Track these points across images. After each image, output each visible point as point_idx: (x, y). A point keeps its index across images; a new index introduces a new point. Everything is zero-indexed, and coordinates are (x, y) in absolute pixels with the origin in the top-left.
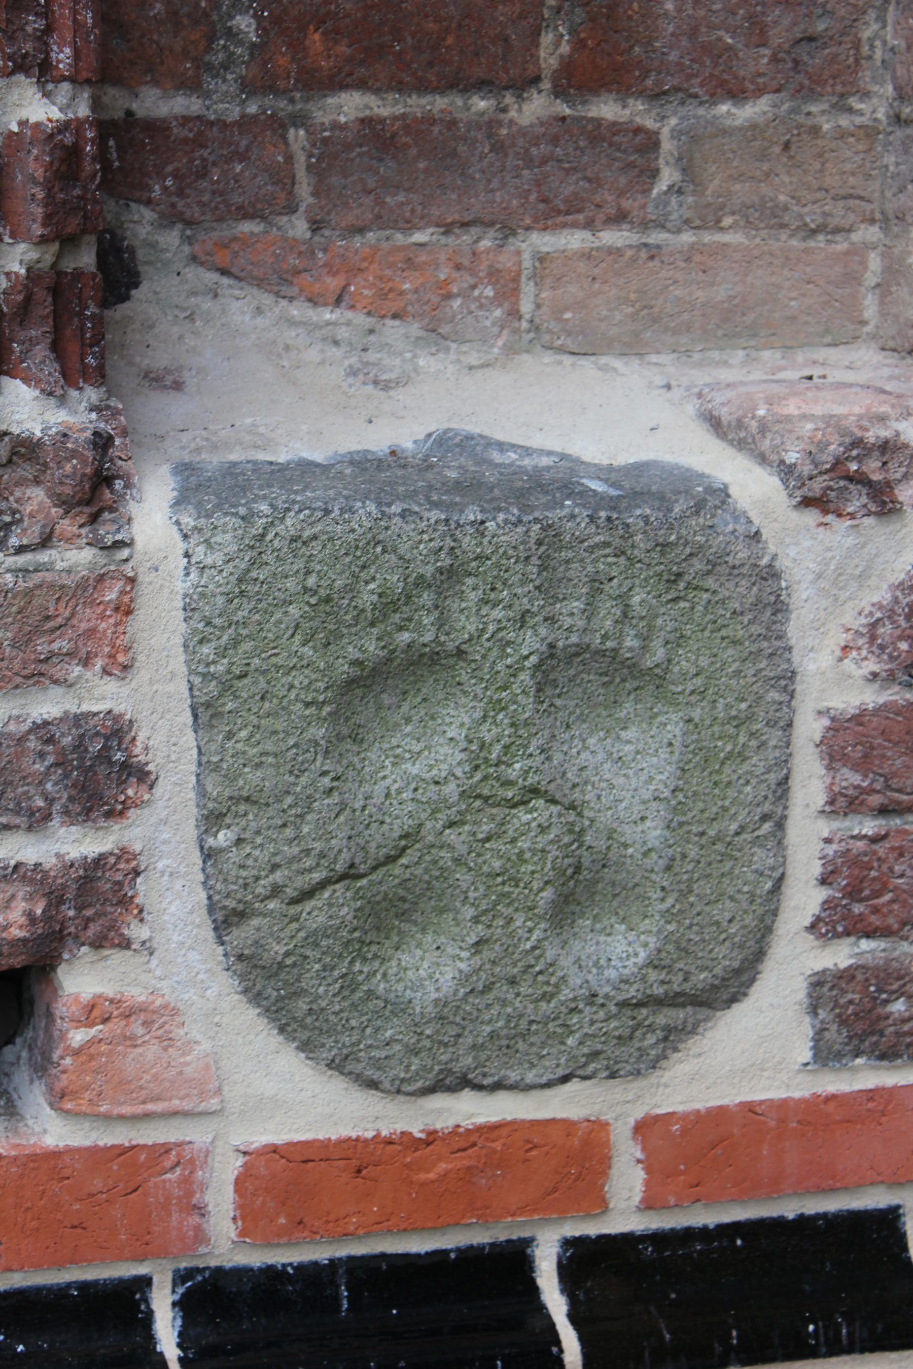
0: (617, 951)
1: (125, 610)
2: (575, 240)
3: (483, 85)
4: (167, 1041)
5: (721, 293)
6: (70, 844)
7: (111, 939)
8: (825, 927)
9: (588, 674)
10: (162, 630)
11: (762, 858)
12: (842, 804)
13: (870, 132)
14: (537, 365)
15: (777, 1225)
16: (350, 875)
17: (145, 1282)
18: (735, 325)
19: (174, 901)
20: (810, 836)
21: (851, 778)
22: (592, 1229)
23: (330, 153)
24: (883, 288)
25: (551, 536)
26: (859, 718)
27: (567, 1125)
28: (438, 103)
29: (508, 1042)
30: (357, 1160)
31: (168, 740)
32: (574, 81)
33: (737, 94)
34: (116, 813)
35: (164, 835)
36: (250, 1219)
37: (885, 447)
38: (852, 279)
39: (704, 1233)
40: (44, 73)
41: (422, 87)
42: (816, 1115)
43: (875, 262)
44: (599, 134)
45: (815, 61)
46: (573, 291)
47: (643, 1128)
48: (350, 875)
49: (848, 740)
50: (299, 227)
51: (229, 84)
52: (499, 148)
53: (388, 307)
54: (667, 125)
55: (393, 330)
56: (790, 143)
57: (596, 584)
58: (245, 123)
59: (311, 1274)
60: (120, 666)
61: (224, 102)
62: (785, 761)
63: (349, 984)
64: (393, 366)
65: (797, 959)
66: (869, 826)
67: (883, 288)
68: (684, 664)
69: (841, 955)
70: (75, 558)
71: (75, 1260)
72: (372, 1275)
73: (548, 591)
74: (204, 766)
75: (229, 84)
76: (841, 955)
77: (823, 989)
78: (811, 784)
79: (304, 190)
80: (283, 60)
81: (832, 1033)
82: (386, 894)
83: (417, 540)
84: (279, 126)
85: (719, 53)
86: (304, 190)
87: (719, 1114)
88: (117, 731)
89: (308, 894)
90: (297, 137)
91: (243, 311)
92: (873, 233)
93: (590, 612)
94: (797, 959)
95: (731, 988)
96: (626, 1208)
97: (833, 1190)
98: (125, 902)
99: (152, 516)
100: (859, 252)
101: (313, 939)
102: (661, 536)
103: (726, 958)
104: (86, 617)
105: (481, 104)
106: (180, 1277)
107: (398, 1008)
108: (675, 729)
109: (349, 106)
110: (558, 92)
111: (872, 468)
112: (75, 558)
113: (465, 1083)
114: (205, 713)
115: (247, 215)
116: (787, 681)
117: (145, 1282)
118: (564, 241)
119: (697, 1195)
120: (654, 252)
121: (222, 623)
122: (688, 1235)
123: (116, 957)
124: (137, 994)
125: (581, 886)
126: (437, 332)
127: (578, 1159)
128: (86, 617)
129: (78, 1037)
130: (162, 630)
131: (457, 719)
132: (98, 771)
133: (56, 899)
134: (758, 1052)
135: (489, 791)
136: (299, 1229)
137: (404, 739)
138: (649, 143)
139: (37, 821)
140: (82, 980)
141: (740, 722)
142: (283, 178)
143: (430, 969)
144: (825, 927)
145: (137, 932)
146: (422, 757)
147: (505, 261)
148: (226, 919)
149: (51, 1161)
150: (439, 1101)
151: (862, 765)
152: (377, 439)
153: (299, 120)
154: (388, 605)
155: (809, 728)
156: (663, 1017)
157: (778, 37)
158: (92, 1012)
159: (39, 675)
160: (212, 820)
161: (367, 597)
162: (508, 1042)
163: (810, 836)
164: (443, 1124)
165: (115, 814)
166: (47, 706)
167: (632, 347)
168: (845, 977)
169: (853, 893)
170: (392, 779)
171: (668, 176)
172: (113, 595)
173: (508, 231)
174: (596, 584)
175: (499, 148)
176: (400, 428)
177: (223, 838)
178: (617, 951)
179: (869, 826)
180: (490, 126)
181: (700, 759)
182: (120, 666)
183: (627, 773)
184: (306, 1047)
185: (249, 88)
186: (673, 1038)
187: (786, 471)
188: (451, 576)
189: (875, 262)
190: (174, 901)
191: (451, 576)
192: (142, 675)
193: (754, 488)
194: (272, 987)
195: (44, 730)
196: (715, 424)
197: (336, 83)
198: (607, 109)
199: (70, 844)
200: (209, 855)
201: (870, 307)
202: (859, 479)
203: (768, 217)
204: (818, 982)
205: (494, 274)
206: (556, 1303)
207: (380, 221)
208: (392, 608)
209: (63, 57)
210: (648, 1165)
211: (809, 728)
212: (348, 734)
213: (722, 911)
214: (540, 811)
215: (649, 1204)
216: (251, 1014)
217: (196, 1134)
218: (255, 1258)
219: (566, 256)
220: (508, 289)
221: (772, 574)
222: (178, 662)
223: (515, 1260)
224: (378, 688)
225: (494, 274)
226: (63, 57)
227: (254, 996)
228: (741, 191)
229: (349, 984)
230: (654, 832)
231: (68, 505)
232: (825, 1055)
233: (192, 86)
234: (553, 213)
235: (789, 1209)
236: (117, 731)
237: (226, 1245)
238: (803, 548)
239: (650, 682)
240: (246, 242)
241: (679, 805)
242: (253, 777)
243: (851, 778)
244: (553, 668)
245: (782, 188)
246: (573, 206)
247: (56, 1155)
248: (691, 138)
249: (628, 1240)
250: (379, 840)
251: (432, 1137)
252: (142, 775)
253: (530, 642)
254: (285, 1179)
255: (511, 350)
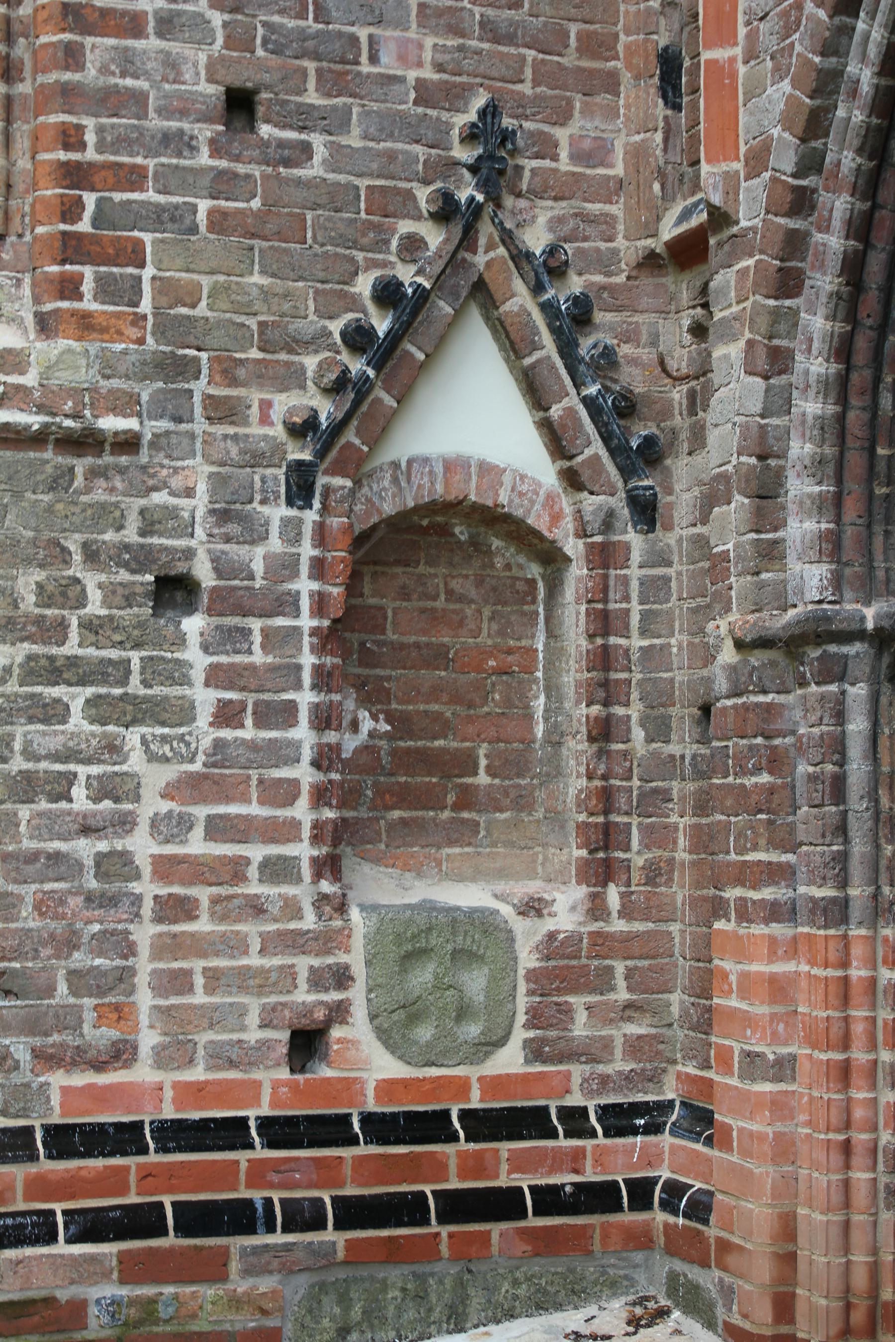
0: (473, 1030)
1: (349, 936)
2: (457, 850)
3: (432, 808)
4: (357, 1049)
5: (498, 865)
6: (334, 996)
7: (343, 1022)
8: (527, 1026)
9: (464, 957)
10: (358, 942)
11: (510, 1006)
12: (530, 993)
13: (538, 821)
14: (447, 884)
15: (515, 1109)
16: (404, 1007)
17: (350, 1115)
18: (502, 874)
19: (359, 1013)
20: (522, 1002)
21: (532, 986)
22: (467, 1107)
23: (392, 826)
24: (543, 864)
25: (454, 920)
26: (534, 969)
27: (460, 1077)
28: (420, 813)
29: (445, 1053)
30: (406, 1084)
31: (359, 970)
32: (457, 807)
33: (501, 811)
34: (346, 989)
35: (357, 995)
36: (378, 1099)
37: (539, 899)
38: (534, 861)
39: (496, 1110)
40: (330, 806)
41: (416, 809)
42: (525, 1078)
43: (540, 857)
44: (463, 821)
45: (522, 802)
46: (457, 864)
47: (480, 1079)
48: (404, 1007)
49: (532, 976)
50: (382, 846)
51: (365, 808)
52: (436, 825)
53: (406, 868)
54: (482, 819)
55: (408, 874)
56: (516, 824)
57: (466, 933)
58: (369, 819)
59: (394, 1115)
60: (348, 951)
61: (364, 813)
62: (515, 980)
63: (404, 1036)
64: (408, 884)
65: (520, 1034)
66: (538, 999)
67: (543, 864)
68: (489, 954)
69: (531, 1034)
70: (338, 923)
71: (334, 1107)
72: (408, 1115)
73: (454, 934)
74: (368, 976)
75: (365, 808)
76: (531, 1034)
77: (527, 1043)
78: (522, 987)
79: (384, 836)
80: (379, 802)
81: (530, 1056)
82: (413, 1011)
83: (421, 920)
84: (377, 819)
85: (495, 800)
86: (384, 836)
87: (500, 1076)
88: (347, 967)
89: (393, 1011)
90: (382, 822)
91: (367, 868)
92: (540, 849)
93: (464, 939)
94: (520, 1034)
95: (502, 1042)
96: (475, 1102)
97: (531, 1099)
98: (348, 1012)
99: (355, 914)
100: (537, 854)
101: (395, 1023)
102: (483, 922)
103: (501, 1033)
104: (340, 938)
105: (432, 813)
106: (361, 1113)
107: (416, 1043)
108: (486, 971)
109: (396, 814)
110: (452, 810)
111: (536, 905)
112: (338, 923)
113: (433, 1064)
114: (368, 963)
115: (368, 843)
116: (515, 959)
117: (350, 1115)
118: (880, 246)
119: (494, 1099)
120: (479, 854)
121: (373, 940)
122: (492, 1110)
123: (345, 1027)
124: (350, 1037)
125: (463, 1013)
126: (420, 875)
127: (462, 1087)
128: (340, 938)
129: (335, 1047)
130: (358, 942)
131: (431, 967)
132: (342, 978)
133: (331, 1010)
134: (509, 1060)
135: (439, 986)
136: (391, 1102)
137: (417, 972)
138: (478, 824)
139: (327, 990)
140: (336, 1032)
141: (503, 969)
142: (379, 833)
143: (424, 1033)
144: (527, 1026)
145: (350, 1020)
146: (423, 977)
147: (438, 856)
148: (373, 1017)
149: (328, 1080)
150: (426, 1069)
151: (535, 982)
152: (406, 901)
153: (383, 818)
154: (414, 936)
155: (521, 972)
156: (485, 1049)
157: (512, 796)
158: (339, 1041)
159: (328, 952)
160: (370, 991)
161: (409, 934)
162: (445, 1053)
163: (522, 1002)
164: (427, 1075)
165: (346, 989)
166: (330, 960)
167: (473, 880)
168: (532, 1040)
169: (534, 1017)
170: (415, 982)
171: (482, 833)
172: (346, 932)
173: (439, 848)
174: (466, 933)
175: (436, 825)
176: (413, 898)
177: (373, 995)
178: (473, 1030)
179: (538, 999)
180: (434, 819)
181: (493, 979)
182: (348, 951)
183: (475, 983)
184: (392, 1053)
185: (370, 809)
186: (487, 1054)
187: (514, 905)
188: (430, 929)
189: (540, 857)
190: (359, 1013)
191: (430, 929)
192: (353, 953)
193: (506, 910)
194: (384, 1036)
195: (329, 966)
196: (496, 896)
197: (392, 808)
198: (465, 815)
199: (334, 996)
200: (369, 1000)
201: (540, 869)
202: (533, 907)
203: (511, 844)
204: (525, 1041)
205: (435, 859)
206: (457, 1125)
207: (404, 845)
208: (412, 941)
209: (334, 802)
210: (481, 1089)
211: (521, 972)
212: (404, 970)
213: (499, 1020)
214: (452, 992)
215: (482, 1100)
216: (378, 1044)
217: (364, 1075)
218: (379, 1110)
219: (455, 855)
220: (439, 864)
221: (511, 931)
222: (362, 950)
223: (446, 1113)
224: (412, 957)
225: (435, 859)
226: (334, 802)
227: (379, 1038)
228: (503, 837)
229: (404, 1036)
230: (482, 998)
231: (336, 910)
232: (527, 1061)
233: (355, 809)
234: (451, 843)
235: (519, 1104)
236: (347, 967)
237: (372, 1106)
238: (519, 925)
239: (481, 959)
240: (369, 850)
241: (488, 991)
242: (380, 980)
243: (532, 986)
244: (456, 954)
245: (514, 836)
246: (457, 841)
247: (329, 1079)
248: (489, 823)
249: (475, 1111)
250: (411, 998)
251: (425, 1079)
252: (352, 979)
253: (449, 947)
254: (387, 1088)
255: (440, 880)
